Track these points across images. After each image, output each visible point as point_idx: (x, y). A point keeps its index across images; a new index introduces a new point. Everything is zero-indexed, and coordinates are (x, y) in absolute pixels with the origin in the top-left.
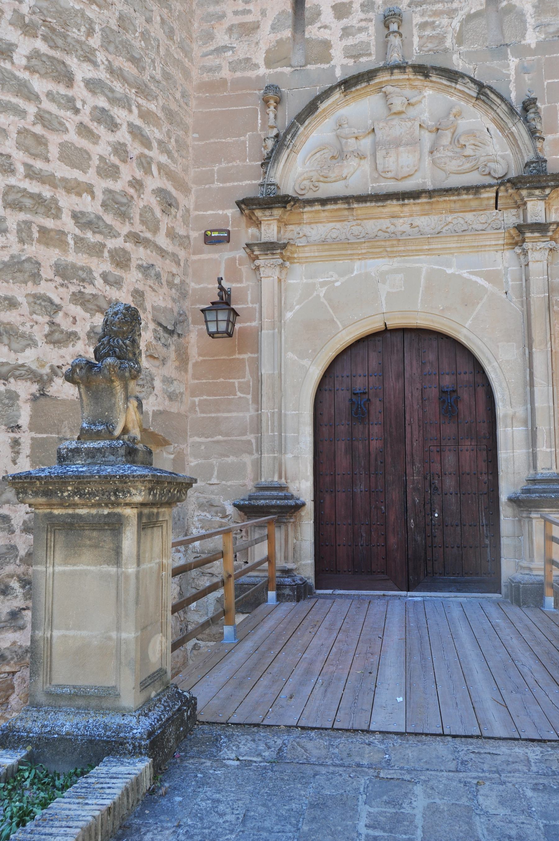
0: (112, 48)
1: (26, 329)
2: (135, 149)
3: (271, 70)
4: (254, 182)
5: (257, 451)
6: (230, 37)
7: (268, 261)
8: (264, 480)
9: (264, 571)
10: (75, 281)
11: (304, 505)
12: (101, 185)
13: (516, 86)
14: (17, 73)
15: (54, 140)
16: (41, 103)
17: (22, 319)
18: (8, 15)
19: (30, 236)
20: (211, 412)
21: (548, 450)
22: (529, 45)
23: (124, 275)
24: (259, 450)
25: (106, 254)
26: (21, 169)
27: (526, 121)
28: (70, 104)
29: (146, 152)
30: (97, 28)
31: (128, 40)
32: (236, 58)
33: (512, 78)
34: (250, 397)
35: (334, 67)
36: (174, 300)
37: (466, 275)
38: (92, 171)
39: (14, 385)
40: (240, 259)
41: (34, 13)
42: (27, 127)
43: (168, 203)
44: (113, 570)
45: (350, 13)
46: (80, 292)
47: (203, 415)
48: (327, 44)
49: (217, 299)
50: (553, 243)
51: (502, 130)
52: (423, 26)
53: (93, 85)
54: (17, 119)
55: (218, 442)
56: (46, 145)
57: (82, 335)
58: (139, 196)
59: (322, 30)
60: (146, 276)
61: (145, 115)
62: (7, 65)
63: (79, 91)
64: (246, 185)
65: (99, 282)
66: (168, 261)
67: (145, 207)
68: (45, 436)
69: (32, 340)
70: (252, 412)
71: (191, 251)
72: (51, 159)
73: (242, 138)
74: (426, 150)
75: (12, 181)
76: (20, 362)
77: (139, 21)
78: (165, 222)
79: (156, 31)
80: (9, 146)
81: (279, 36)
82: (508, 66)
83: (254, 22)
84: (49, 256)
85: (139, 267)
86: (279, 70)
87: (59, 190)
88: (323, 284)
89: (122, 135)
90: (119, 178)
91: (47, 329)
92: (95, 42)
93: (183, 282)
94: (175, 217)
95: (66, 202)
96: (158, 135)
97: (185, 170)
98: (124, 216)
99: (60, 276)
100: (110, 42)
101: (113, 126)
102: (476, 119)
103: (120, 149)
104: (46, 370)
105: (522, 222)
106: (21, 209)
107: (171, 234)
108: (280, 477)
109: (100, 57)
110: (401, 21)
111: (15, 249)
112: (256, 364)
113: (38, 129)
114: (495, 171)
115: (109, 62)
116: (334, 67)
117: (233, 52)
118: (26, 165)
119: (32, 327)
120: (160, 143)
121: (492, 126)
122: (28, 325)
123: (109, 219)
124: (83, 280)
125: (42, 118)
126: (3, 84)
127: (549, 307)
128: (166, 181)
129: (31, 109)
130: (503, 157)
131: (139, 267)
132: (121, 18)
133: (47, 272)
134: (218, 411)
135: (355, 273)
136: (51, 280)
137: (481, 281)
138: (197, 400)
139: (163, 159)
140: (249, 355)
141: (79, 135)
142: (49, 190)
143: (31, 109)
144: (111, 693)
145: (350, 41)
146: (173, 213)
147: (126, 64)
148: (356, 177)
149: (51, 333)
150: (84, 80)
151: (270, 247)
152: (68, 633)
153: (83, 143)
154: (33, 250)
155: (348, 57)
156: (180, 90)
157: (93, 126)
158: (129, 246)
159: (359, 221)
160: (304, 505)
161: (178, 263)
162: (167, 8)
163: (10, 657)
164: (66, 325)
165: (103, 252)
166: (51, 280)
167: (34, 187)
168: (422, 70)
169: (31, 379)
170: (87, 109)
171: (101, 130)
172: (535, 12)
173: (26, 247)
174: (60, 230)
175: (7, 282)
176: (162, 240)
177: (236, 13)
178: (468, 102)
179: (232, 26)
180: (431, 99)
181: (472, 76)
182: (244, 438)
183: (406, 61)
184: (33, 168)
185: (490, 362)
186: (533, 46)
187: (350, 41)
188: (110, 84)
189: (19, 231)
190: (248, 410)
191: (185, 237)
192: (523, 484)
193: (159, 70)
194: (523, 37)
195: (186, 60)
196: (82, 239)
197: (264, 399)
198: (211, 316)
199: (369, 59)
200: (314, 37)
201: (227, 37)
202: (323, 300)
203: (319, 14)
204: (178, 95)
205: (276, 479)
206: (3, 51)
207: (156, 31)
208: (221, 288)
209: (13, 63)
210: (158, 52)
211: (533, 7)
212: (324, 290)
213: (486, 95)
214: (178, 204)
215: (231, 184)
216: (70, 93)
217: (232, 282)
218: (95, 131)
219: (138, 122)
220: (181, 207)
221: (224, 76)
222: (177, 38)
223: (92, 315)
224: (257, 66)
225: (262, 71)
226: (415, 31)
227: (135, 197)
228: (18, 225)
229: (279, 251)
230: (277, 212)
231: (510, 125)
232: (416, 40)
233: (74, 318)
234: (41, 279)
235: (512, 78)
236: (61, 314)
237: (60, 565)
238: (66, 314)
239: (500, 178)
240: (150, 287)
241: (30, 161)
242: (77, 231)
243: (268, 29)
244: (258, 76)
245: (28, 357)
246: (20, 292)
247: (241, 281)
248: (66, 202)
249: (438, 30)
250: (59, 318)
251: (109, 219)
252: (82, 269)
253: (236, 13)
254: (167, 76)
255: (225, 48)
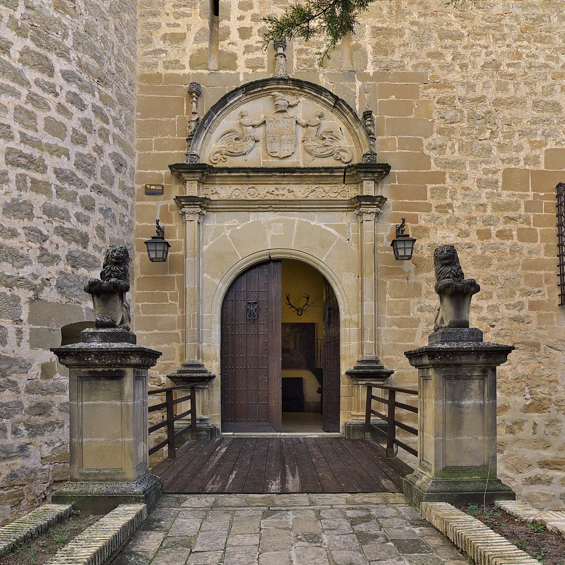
0: (80, 48)
1: (24, 252)
2: (97, 124)
3: (194, 71)
4: (181, 151)
5: (183, 341)
6: (164, 43)
7: (191, 209)
8: (187, 361)
9: (188, 420)
10: (57, 218)
11: (214, 377)
12: (74, 149)
13: (359, 101)
14: (13, 64)
15: (41, 115)
16: (30, 88)
17: (21, 245)
18: (6, 19)
19: (25, 186)
20: (150, 313)
21: (371, 342)
22: (369, 73)
23: (90, 215)
24: (184, 340)
25: (78, 200)
26: (18, 136)
27: (365, 126)
28: (52, 90)
29: (105, 126)
30: (70, 32)
31: (92, 42)
32: (168, 59)
33: (357, 95)
34: (177, 303)
35: (239, 73)
36: (124, 234)
37: (323, 227)
38: (68, 139)
39: (17, 291)
40: (171, 206)
41: (24, 19)
42: (21, 105)
43: (120, 165)
44: (118, 403)
45: (251, 36)
46: (61, 226)
47: (144, 315)
48: (234, 57)
49: (156, 235)
50: (379, 209)
51: (349, 129)
52: (300, 51)
53: (68, 76)
54: (14, 98)
55: (155, 334)
56: (35, 119)
57: (63, 257)
58: (100, 159)
59: (231, 45)
60: (106, 217)
61: (104, 99)
62: (6, 58)
63: (58, 80)
64: (175, 153)
65: (74, 219)
66: (120, 206)
67: (104, 166)
68: (39, 327)
69: (28, 260)
70: (179, 313)
71: (135, 198)
72: (39, 129)
73: (173, 119)
74: (300, 139)
75: (11, 145)
76: (21, 275)
77: (100, 28)
78: (118, 177)
79: (113, 37)
80: (8, 119)
81: (200, 46)
82: (355, 86)
83: (182, 33)
84: (38, 200)
85: (101, 209)
86: (200, 71)
87: (45, 152)
88: (229, 227)
89: (89, 113)
90: (86, 145)
91: (38, 253)
92: (69, 42)
93: (130, 221)
94: (125, 174)
95: (51, 162)
96: (113, 114)
97: (132, 139)
98: (90, 173)
99: (46, 215)
100: (79, 43)
101: (82, 107)
102: (333, 121)
103: (87, 124)
104: (38, 282)
105: (360, 194)
106: (18, 166)
107: (123, 187)
108: (199, 358)
109: (73, 55)
110: (286, 46)
111: (15, 194)
112: (182, 282)
113: (29, 107)
114: (344, 158)
115: (79, 58)
116: (239, 73)
117: (166, 54)
118: (20, 133)
119: (28, 250)
120: (115, 119)
121: (343, 127)
122: (25, 249)
123: (80, 174)
124: (63, 219)
125: (32, 98)
126: (3, 72)
127: (374, 251)
128: (118, 147)
129: (24, 92)
130: (349, 148)
131: (101, 209)
132: (87, 25)
133: (37, 212)
134: (156, 313)
135: (251, 221)
136: (40, 218)
137: (333, 231)
138: (140, 304)
139: (116, 131)
140: (177, 274)
141: (58, 112)
142: (38, 152)
143: (24, 92)
144: (119, 471)
145: (250, 56)
146: (124, 171)
147: (90, 60)
148: (255, 158)
149: (43, 255)
150: (61, 71)
151: (192, 200)
152: (92, 439)
153: (60, 118)
154: (27, 195)
155: (248, 67)
156: (128, 79)
157: (68, 106)
158: (94, 194)
159: (254, 185)
160: (214, 377)
161: (127, 208)
162: (119, 18)
163: (20, 475)
164: (51, 250)
165: (76, 199)
166: (40, 218)
167: (27, 150)
168: (299, 84)
169: (28, 288)
170: (63, 94)
171: (73, 109)
172: (373, 52)
173: (22, 193)
174: (46, 182)
175: (10, 218)
176: (116, 190)
177: (168, 25)
178: (328, 108)
179: (166, 34)
180: (305, 107)
181: (331, 91)
182: (173, 331)
183: (288, 75)
184: (26, 136)
185: (337, 285)
186: (371, 74)
187: (250, 56)
188: (79, 75)
189: (18, 182)
190: (176, 313)
191: (131, 188)
192: (356, 364)
193: (113, 65)
194: (365, 68)
195: (132, 57)
196: (62, 188)
197: (188, 305)
198: (152, 247)
199: (263, 70)
200: (225, 50)
201: (162, 43)
202: (228, 238)
203: (229, 34)
204: (127, 84)
205: (196, 360)
206: (5, 47)
207: (113, 37)
208: (159, 227)
209: (10, 56)
210: (113, 52)
211: (372, 47)
212: (229, 231)
213: (340, 106)
214: (126, 164)
215: (165, 152)
216: (52, 81)
217: (165, 223)
218: (69, 109)
219: (99, 104)
220: (129, 167)
221: (160, 72)
222: (126, 40)
223: (69, 243)
224: (183, 67)
225: (187, 71)
226: (295, 54)
227: (98, 159)
228: (17, 177)
229: (199, 203)
230: (198, 176)
231: (355, 127)
232: (295, 61)
233: (57, 245)
234: (34, 217)
235: (357, 95)
236: (48, 242)
237: (86, 401)
238: (52, 242)
239: (347, 163)
240: (108, 224)
241: (24, 131)
242: (58, 183)
243: (192, 40)
244: (184, 74)
245: (26, 272)
246: (18, 224)
247: (172, 223)
248: (51, 162)
249: (310, 56)
250: (46, 245)
251: (80, 174)
252: (61, 210)
253: (168, 25)
254: (119, 70)
255: (161, 51)
